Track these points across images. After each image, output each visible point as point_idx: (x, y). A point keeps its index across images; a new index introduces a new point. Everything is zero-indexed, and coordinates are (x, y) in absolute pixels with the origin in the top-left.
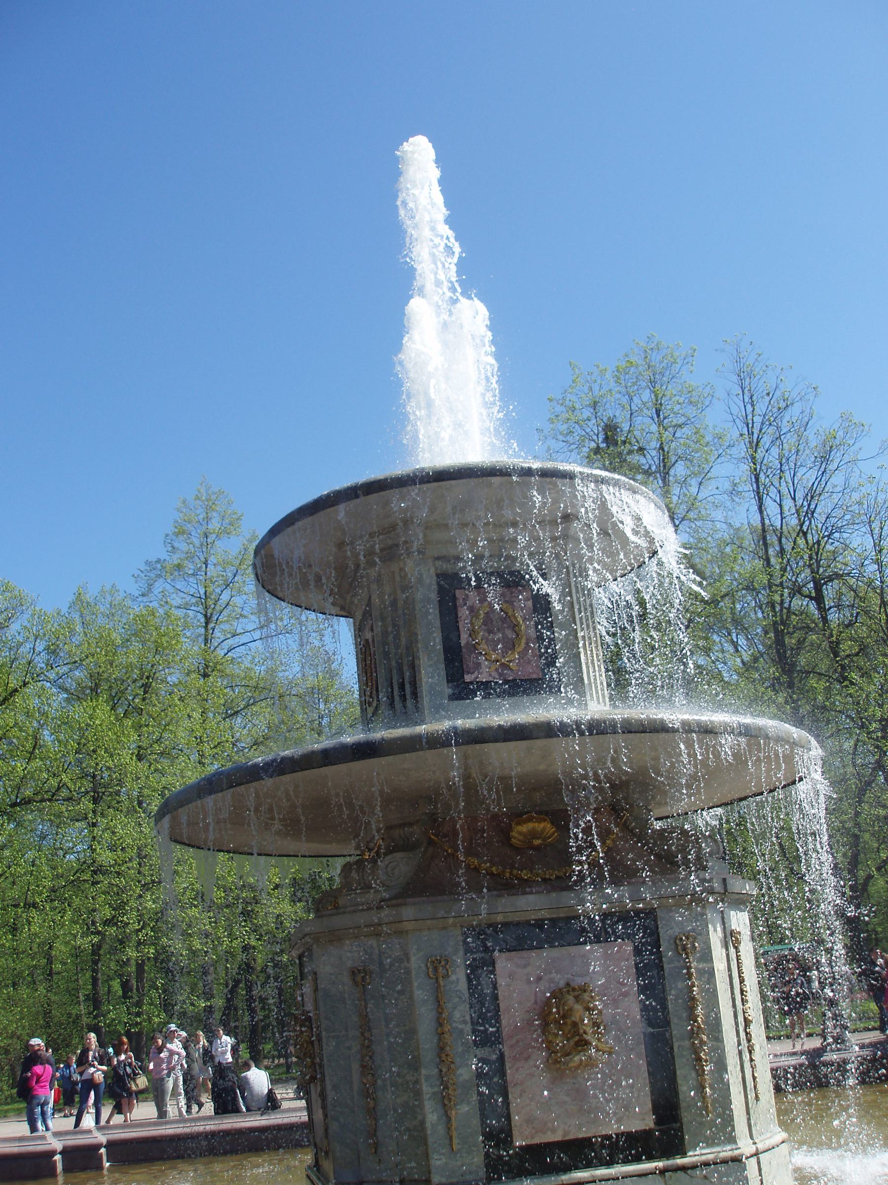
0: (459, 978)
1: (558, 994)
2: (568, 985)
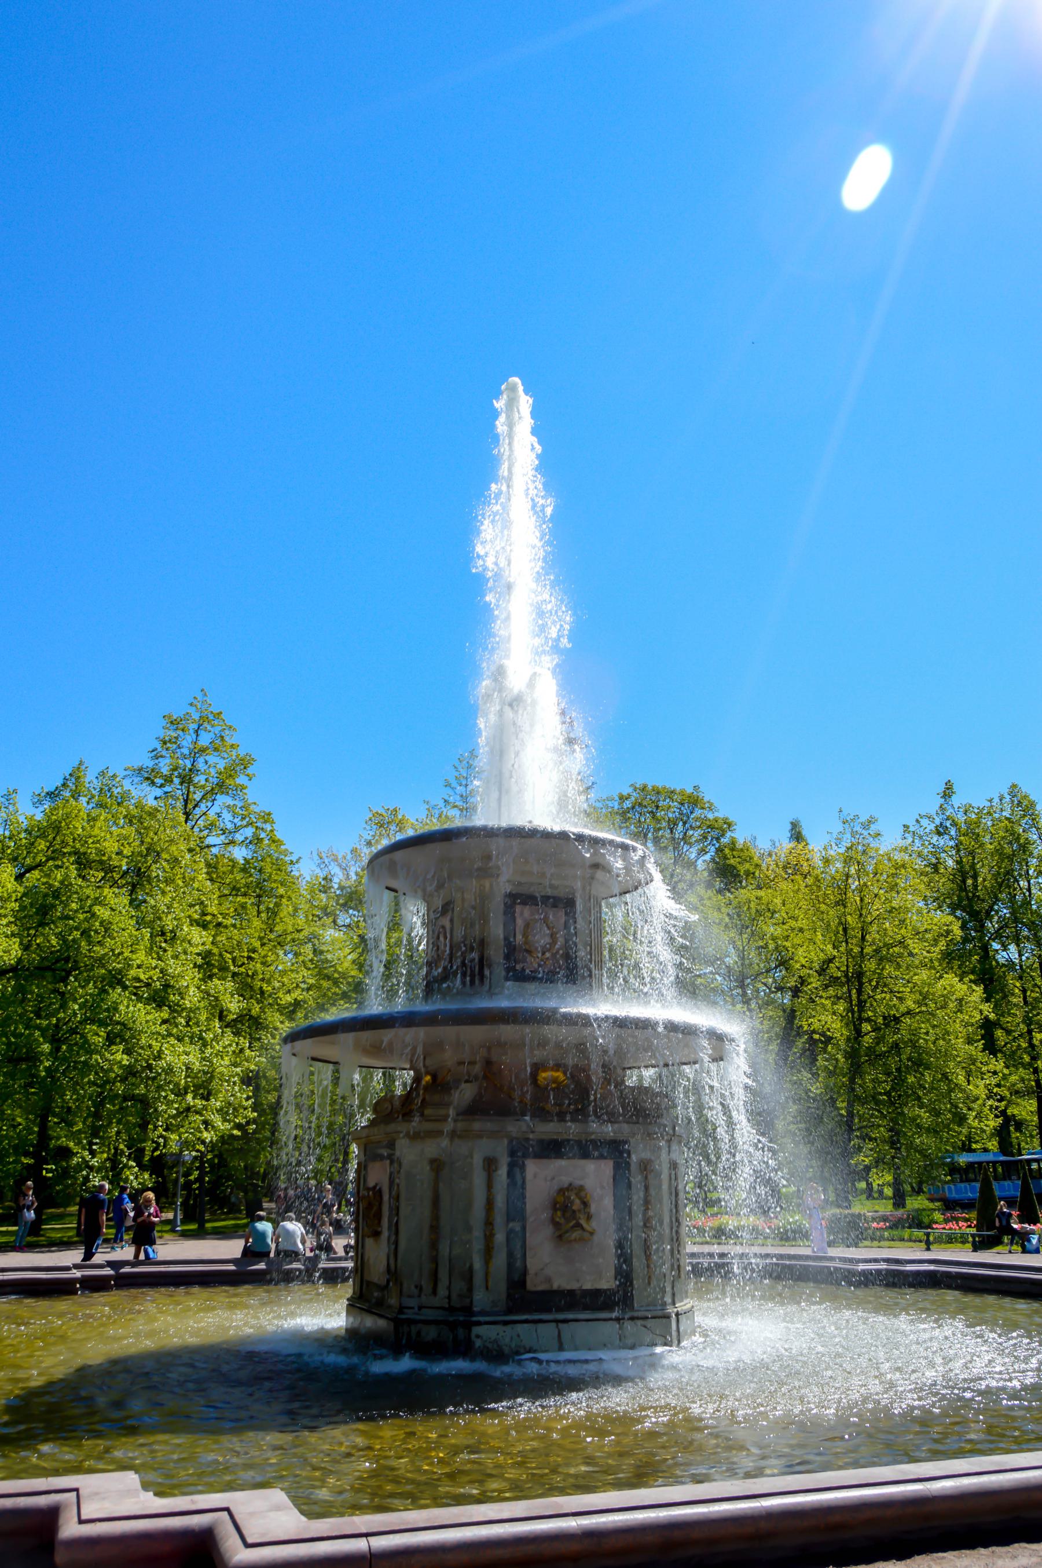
0: (503, 1172)
1: (561, 1191)
2: (570, 1185)
